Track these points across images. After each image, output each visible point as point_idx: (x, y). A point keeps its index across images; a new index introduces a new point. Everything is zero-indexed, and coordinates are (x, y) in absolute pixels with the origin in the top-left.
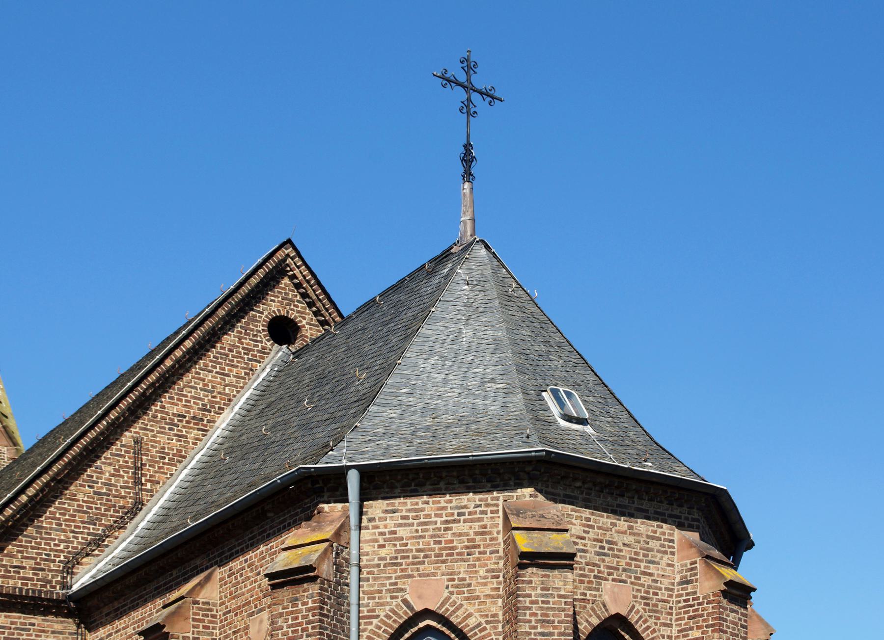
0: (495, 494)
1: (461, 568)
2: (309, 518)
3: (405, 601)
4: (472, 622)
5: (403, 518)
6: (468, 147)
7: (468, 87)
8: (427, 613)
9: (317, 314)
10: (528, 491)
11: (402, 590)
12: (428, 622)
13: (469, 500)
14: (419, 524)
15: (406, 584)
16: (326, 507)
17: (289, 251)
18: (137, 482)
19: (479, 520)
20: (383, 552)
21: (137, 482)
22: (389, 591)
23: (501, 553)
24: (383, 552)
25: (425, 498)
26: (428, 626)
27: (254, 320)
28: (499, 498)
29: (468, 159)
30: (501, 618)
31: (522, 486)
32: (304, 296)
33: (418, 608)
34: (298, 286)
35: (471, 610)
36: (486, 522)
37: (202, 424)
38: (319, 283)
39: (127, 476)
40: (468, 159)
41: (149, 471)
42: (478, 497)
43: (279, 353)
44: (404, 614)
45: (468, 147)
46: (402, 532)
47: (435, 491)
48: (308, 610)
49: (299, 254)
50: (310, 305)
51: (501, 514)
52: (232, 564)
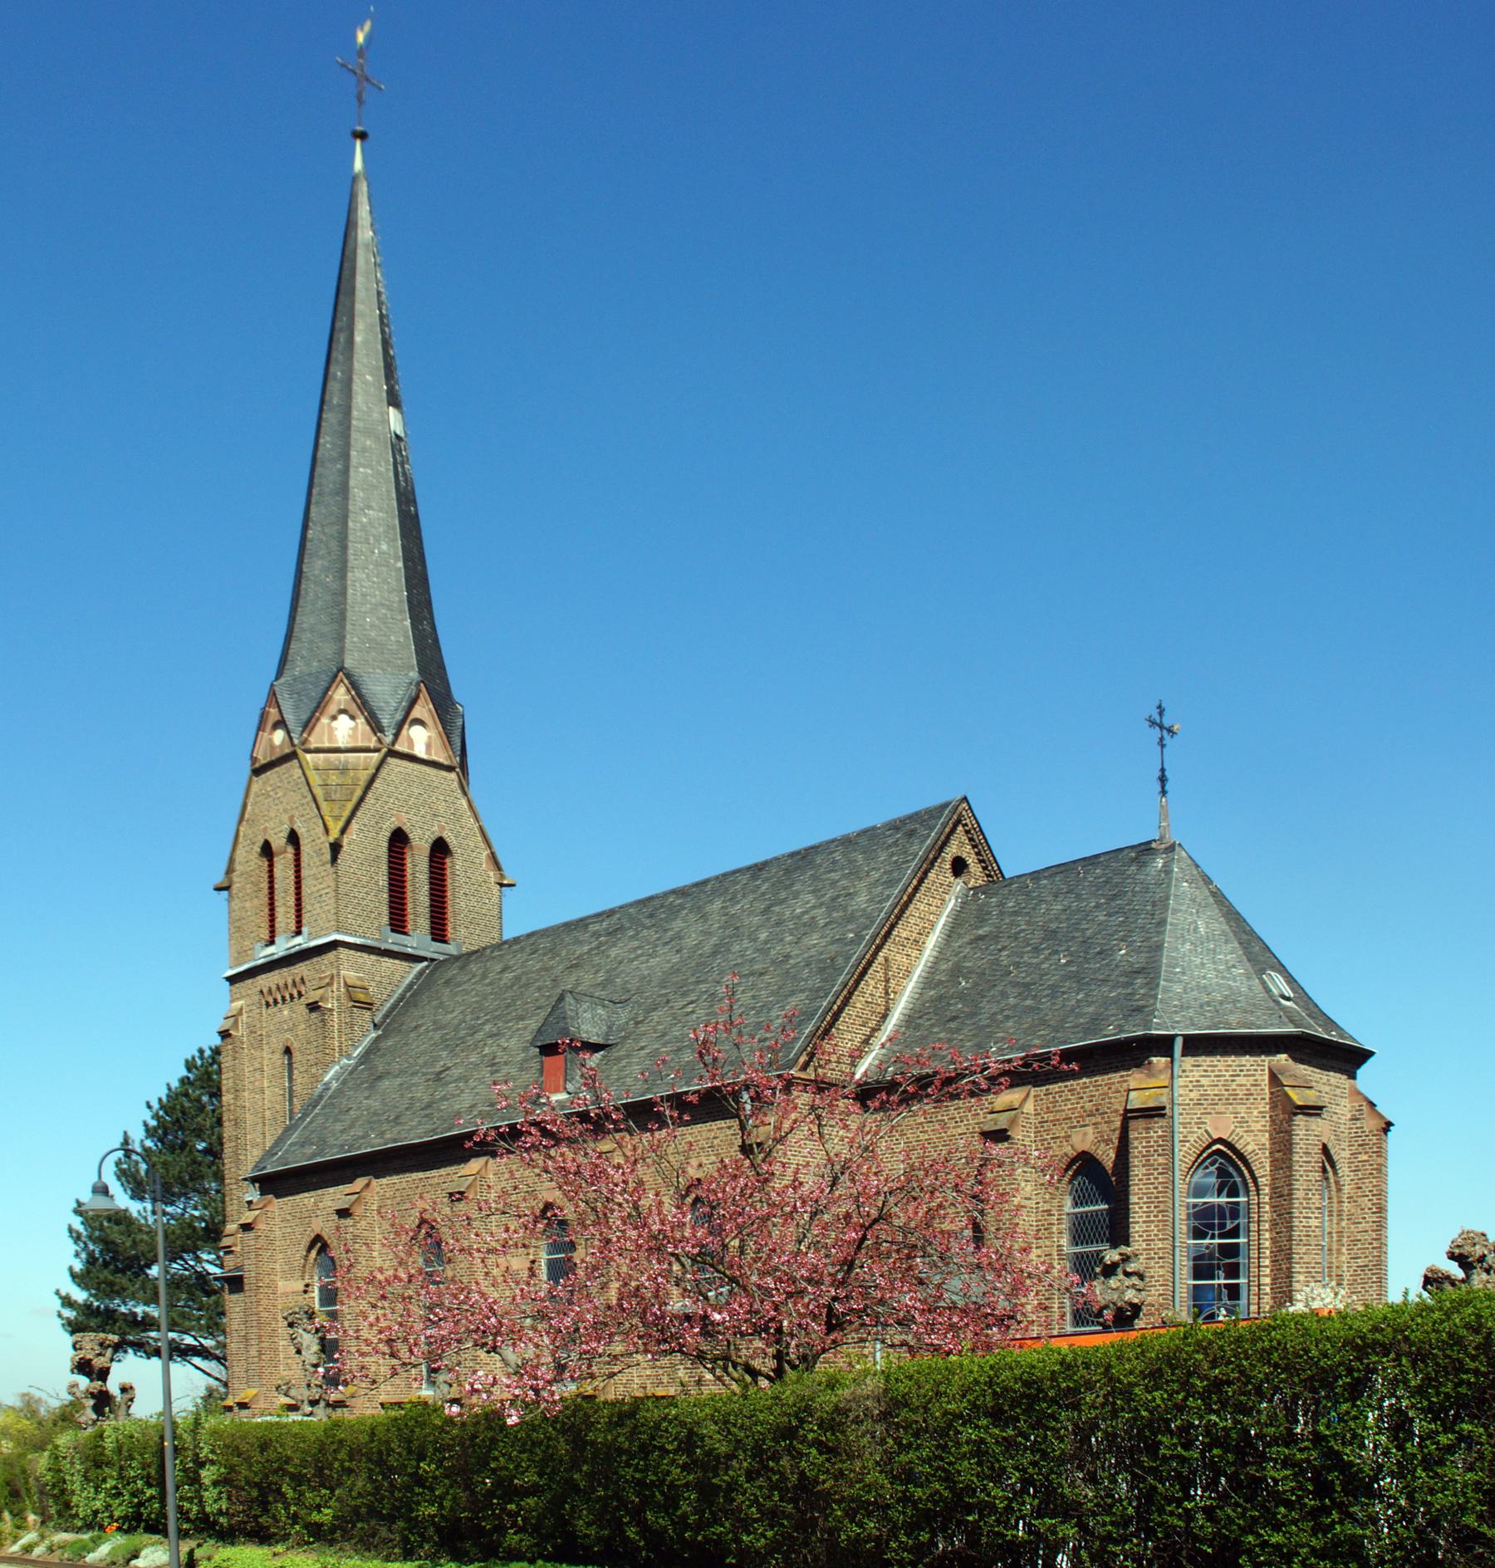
0: (1263, 1057)
1: (1242, 1109)
2: (1138, 1066)
3: (1206, 1131)
4: (1250, 1148)
5: (1205, 1071)
6: (1163, 770)
7: (1161, 727)
8: (1220, 1141)
9: (978, 854)
10: (1284, 1056)
11: (1205, 1123)
12: (1222, 1148)
13: (1247, 1060)
14: (1216, 1076)
15: (1207, 1119)
16: (1154, 1059)
17: (964, 805)
18: (887, 993)
19: (1253, 1075)
20: (1192, 1095)
21: (887, 993)
22: (1196, 1123)
23: (1267, 1100)
24: (1192, 1095)
25: (1218, 1057)
26: (1218, 1150)
27: (944, 860)
28: (1265, 1060)
29: (1163, 779)
30: (1268, 1146)
31: (1279, 1053)
32: (971, 839)
33: (1215, 1136)
34: (967, 832)
35: (1249, 1140)
36: (1257, 1077)
37: (918, 944)
38: (981, 830)
39: (881, 988)
40: (1163, 779)
41: (892, 983)
42: (1252, 1059)
43: (958, 885)
44: (1206, 1140)
45: (1163, 770)
46: (1204, 1081)
47: (1225, 1053)
48: (1159, 1137)
49: (970, 808)
50: (974, 847)
51: (1267, 1072)
52: (1051, 1087)
